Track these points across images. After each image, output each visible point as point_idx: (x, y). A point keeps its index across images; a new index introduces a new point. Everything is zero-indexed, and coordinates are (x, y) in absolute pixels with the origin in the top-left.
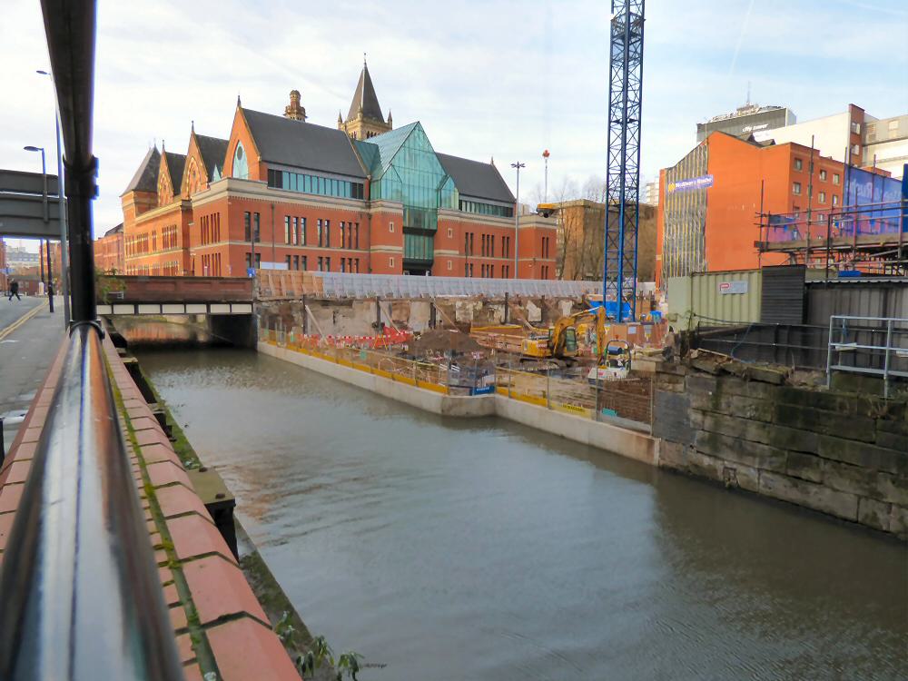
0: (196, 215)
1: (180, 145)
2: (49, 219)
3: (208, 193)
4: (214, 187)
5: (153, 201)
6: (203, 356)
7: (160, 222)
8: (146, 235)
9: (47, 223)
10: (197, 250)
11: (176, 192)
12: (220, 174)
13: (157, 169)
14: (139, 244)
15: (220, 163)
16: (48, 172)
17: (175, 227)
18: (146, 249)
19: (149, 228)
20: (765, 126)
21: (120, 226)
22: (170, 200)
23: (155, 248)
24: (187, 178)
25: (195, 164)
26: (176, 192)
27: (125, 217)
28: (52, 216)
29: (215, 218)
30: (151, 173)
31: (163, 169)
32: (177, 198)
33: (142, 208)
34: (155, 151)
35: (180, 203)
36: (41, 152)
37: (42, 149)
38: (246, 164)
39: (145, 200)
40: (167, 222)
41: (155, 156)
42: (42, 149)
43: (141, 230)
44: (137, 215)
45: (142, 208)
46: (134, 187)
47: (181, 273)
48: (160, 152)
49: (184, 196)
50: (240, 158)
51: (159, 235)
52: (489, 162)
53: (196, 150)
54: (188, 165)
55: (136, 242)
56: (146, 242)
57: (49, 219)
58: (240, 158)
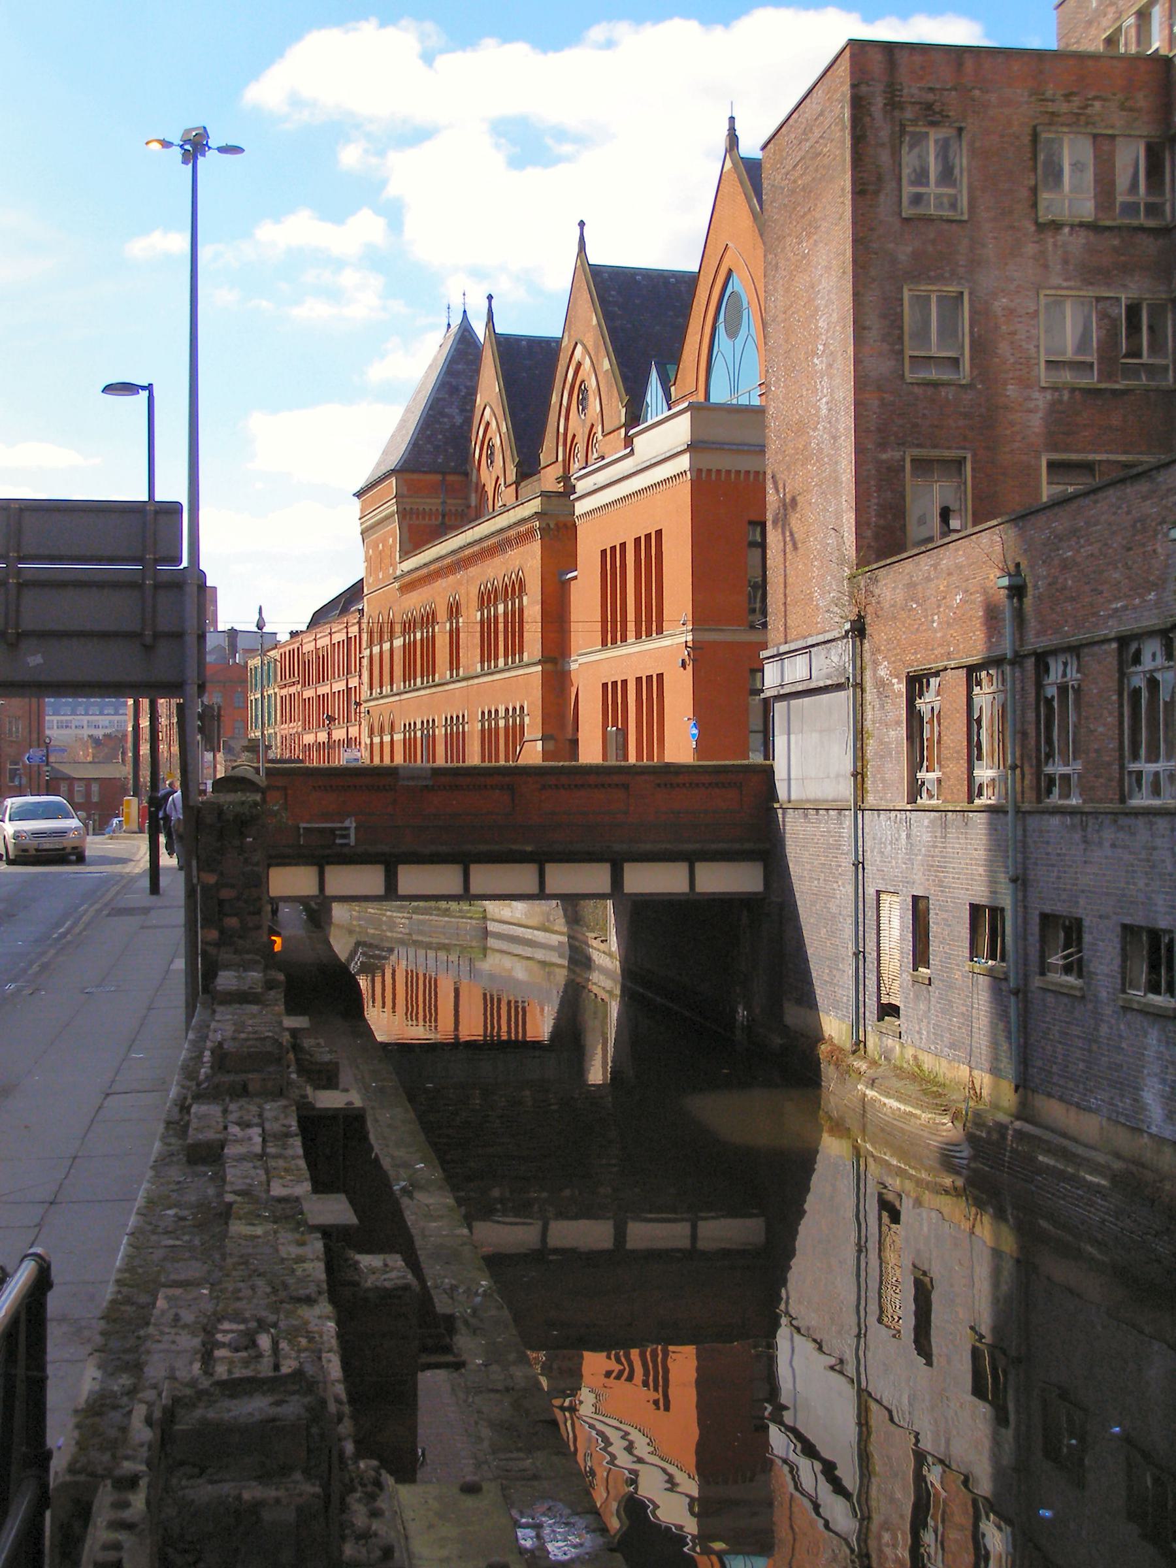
0: (589, 547)
1: (539, 302)
2: (156, 636)
3: (627, 466)
4: (649, 444)
5: (453, 504)
6: (1167, 32)
7: (473, 571)
8: (429, 619)
9: (148, 649)
10: (593, 664)
11: (528, 468)
12: (668, 395)
13: (472, 392)
14: (408, 648)
15: (669, 356)
16: (163, 494)
17: (517, 588)
18: (430, 668)
19: (437, 594)
20: (783, 1291)
21: (355, 592)
22: (508, 495)
23: (454, 661)
24: (567, 421)
25: (591, 363)
26: (528, 468)
27: (368, 559)
28: (163, 625)
29: (650, 547)
30: (454, 411)
31: (489, 389)
32: (528, 487)
33: (419, 529)
34: (465, 335)
35: (534, 506)
36: (145, 394)
37: (149, 388)
38: (751, 351)
39: (432, 503)
40: (495, 570)
41: (464, 352)
42: (149, 388)
43: (415, 602)
44: (406, 554)
45: (416, 536)
46: (393, 461)
47: (533, 753)
48: (480, 329)
49: (549, 479)
50: (732, 333)
51: (472, 616)
52: (419, 1476)
53: (590, 319)
54: (563, 373)
55: (398, 643)
56: (430, 644)
57: (156, 636)
58: (732, 333)
